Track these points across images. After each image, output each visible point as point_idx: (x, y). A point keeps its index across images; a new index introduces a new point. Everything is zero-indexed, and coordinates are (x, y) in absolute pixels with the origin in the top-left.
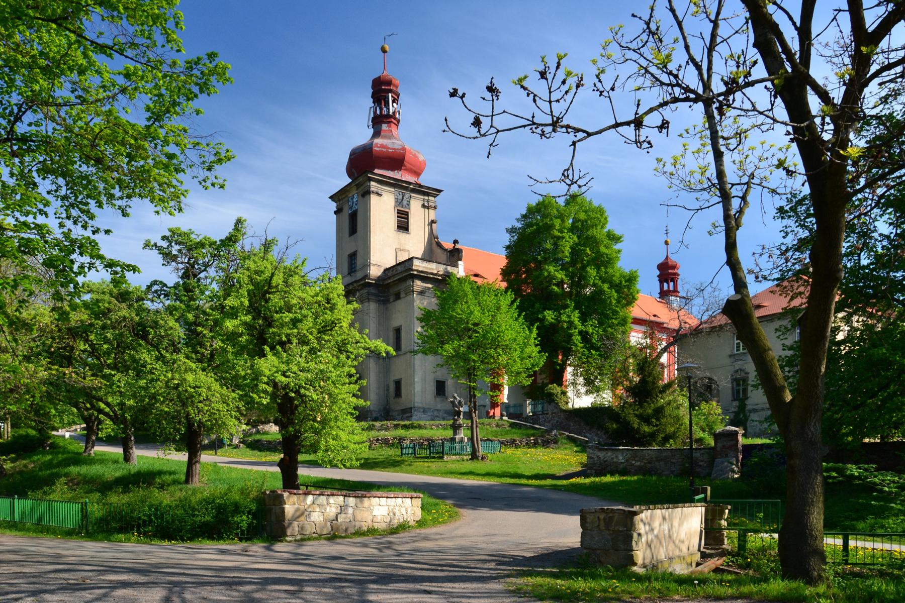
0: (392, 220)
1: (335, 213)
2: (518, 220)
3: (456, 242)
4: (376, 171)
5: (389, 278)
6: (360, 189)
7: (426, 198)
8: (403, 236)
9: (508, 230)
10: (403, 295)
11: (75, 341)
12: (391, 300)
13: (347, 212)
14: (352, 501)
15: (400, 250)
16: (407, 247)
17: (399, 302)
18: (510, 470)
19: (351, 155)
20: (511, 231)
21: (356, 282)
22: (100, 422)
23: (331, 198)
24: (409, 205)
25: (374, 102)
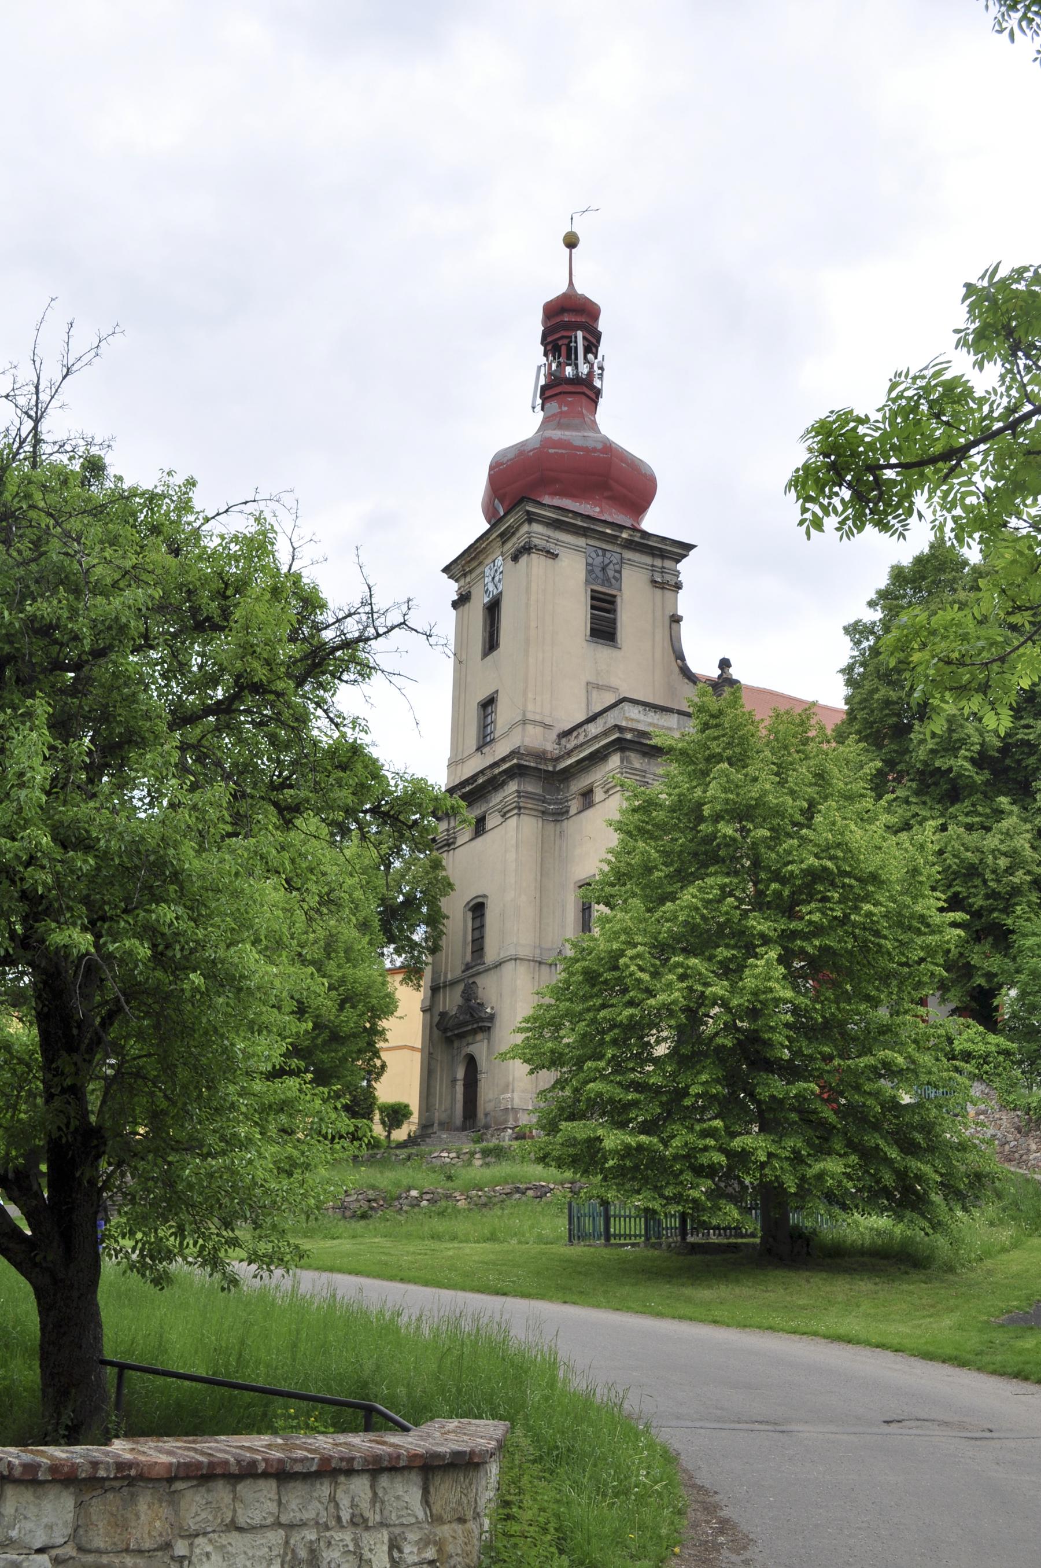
0: (577, 614)
1: (455, 605)
2: (872, 604)
3: (725, 664)
4: (547, 500)
5: (569, 754)
6: (509, 545)
7: (658, 562)
8: (604, 652)
9: (847, 630)
10: (598, 795)
11: (768, 1085)
12: (573, 811)
13: (480, 600)
14: (486, 600)
15: (598, 687)
16: (614, 682)
17: (590, 813)
18: (870, 1286)
19: (491, 468)
20: (856, 631)
21: (496, 764)
22: (141, 1068)
23: (446, 570)
24: (619, 580)
25: (546, 354)
